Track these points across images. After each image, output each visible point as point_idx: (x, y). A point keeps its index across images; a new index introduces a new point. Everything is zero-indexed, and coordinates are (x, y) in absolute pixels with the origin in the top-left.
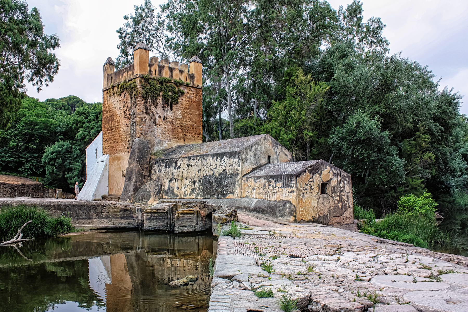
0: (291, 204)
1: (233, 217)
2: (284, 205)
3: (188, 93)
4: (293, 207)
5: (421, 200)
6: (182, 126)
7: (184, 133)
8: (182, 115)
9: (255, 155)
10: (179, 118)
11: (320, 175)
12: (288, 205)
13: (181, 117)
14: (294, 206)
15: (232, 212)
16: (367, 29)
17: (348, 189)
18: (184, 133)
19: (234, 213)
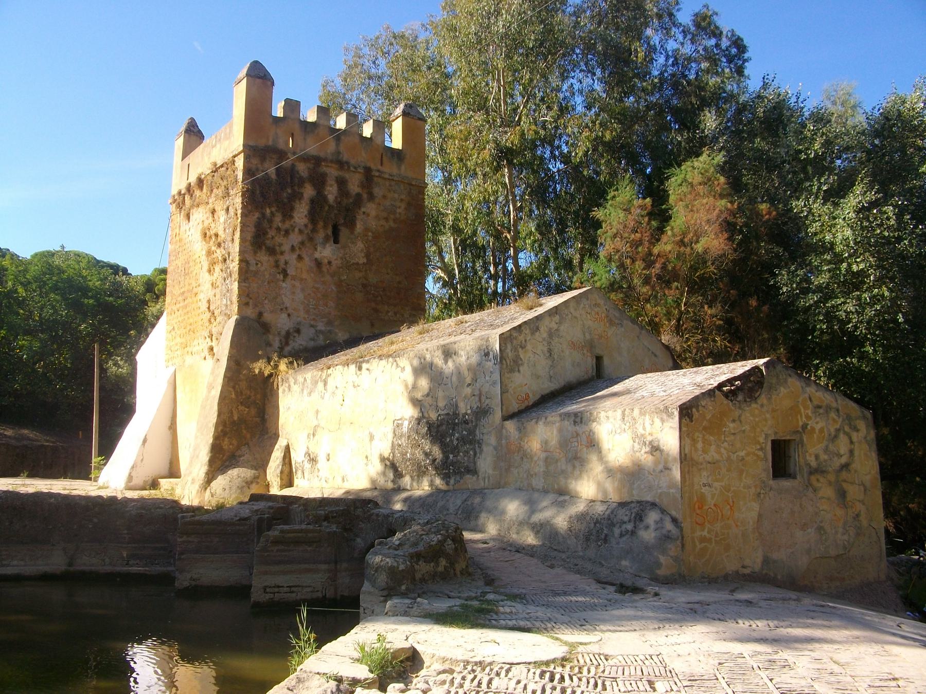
0: (663, 511)
1: (443, 562)
2: (639, 518)
3: (384, 197)
4: (669, 526)
5: (427, 488)
6: (364, 286)
7: (373, 305)
8: (367, 255)
9: (550, 351)
10: (358, 264)
11: (719, 328)
12: (652, 517)
13: (362, 260)
14: (674, 520)
15: (441, 543)
16: (876, 137)
17: (867, 466)
18: (373, 305)
19: (449, 546)
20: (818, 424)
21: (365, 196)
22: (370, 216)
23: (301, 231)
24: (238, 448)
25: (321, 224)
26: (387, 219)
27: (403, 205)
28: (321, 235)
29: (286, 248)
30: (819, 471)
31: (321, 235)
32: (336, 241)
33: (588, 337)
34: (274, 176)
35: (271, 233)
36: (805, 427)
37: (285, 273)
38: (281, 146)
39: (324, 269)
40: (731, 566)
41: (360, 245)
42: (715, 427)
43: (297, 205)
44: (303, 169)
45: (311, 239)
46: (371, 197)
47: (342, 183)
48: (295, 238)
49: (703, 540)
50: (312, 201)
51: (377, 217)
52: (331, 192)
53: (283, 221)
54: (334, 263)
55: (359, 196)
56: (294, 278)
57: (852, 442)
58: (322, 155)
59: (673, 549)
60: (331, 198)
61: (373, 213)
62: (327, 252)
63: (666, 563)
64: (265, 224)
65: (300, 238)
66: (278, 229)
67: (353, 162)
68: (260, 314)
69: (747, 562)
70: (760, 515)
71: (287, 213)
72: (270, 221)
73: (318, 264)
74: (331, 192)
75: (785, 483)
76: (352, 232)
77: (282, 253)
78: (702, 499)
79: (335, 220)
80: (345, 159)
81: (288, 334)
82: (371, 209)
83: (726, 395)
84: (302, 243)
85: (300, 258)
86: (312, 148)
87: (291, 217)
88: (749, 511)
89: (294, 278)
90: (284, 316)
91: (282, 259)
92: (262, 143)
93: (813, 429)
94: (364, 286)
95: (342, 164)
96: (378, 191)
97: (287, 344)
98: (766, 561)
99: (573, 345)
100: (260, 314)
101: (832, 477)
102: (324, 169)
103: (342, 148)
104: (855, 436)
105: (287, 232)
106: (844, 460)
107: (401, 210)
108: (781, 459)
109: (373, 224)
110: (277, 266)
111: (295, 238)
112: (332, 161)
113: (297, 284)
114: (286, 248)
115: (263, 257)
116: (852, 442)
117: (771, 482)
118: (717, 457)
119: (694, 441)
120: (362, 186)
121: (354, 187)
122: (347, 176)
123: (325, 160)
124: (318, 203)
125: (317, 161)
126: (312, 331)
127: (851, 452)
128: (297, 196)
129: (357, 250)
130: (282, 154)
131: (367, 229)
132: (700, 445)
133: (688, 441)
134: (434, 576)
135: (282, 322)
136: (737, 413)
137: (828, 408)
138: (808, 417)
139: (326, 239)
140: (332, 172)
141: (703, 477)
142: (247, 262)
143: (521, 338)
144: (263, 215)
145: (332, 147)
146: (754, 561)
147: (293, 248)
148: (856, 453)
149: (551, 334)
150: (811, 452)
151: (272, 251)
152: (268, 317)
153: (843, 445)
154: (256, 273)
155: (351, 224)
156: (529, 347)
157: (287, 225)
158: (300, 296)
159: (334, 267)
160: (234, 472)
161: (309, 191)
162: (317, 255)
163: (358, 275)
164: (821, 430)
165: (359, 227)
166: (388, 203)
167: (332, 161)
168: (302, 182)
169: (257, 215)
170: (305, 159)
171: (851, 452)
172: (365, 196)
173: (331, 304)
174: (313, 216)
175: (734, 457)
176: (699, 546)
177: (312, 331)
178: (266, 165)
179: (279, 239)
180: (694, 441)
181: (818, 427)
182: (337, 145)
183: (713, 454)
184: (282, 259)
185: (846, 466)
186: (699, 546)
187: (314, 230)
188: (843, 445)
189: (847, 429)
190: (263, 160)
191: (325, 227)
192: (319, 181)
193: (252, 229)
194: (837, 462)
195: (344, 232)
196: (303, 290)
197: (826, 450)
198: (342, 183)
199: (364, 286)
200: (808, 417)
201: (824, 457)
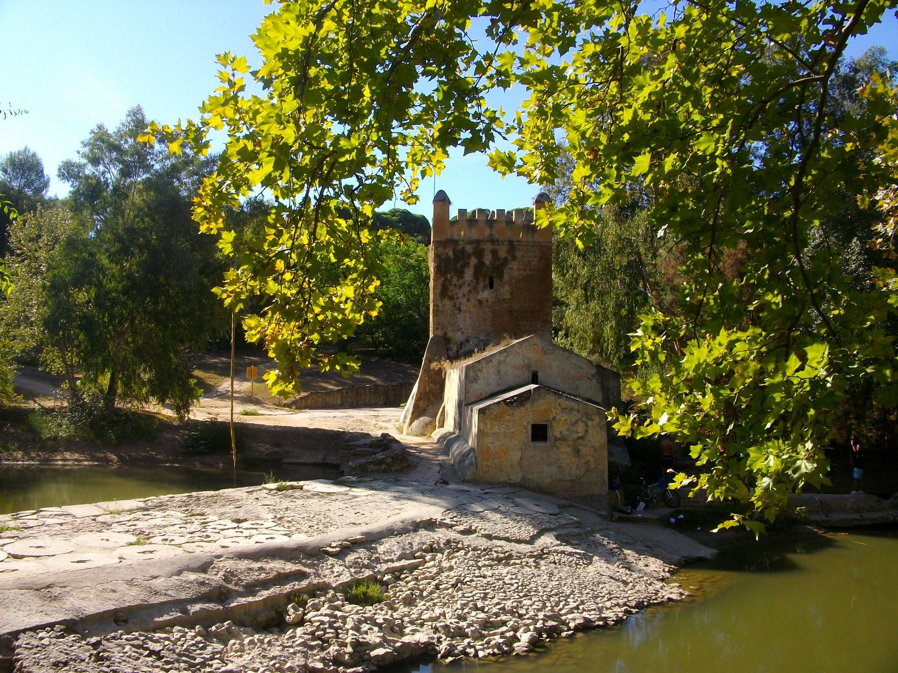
3: (523, 256)
8: (511, 294)
9: (499, 372)
13: (508, 297)
20: (563, 417)
21: (510, 258)
22: (513, 270)
23: (469, 285)
24: (428, 406)
25: (481, 279)
26: (525, 270)
27: (536, 260)
28: (482, 284)
29: (460, 295)
30: (563, 439)
31: (482, 284)
32: (491, 287)
33: (526, 362)
34: (452, 256)
35: (451, 288)
36: (554, 418)
37: (460, 310)
38: (456, 237)
39: (484, 305)
40: (502, 479)
41: (507, 288)
42: (498, 418)
43: (466, 270)
44: (469, 249)
45: (475, 288)
46: (514, 258)
47: (494, 253)
48: (465, 289)
49: (487, 466)
50: (476, 267)
51: (518, 269)
52: (488, 259)
53: (458, 280)
54: (490, 300)
55: (506, 258)
56: (465, 312)
57: (587, 426)
58: (481, 238)
59: (472, 469)
60: (487, 263)
61: (515, 267)
62: (485, 294)
63: (469, 475)
64: (447, 283)
65: (468, 289)
66: (455, 285)
67: (501, 239)
68: (445, 333)
69: (512, 478)
70: (521, 458)
71: (460, 274)
72: (450, 281)
73: (480, 302)
74: (488, 259)
75: (540, 444)
76: (502, 281)
77: (458, 298)
78: (488, 449)
79: (490, 276)
80: (496, 237)
81: (462, 343)
82: (514, 265)
83: (507, 404)
84: (470, 291)
85: (468, 300)
86: (475, 235)
87: (463, 277)
88: (515, 456)
89: (465, 312)
90: (460, 333)
91: (458, 302)
92: (444, 238)
93: (560, 420)
94: (510, 312)
95: (493, 241)
96: (518, 254)
97: (461, 348)
98: (524, 478)
99: (515, 367)
100: (445, 333)
101: (571, 443)
102: (482, 246)
103: (494, 232)
104: (590, 423)
105: (460, 286)
106: (580, 435)
107: (535, 262)
108: (539, 432)
109: (515, 274)
110: (455, 306)
111: (465, 289)
112: (487, 241)
113: (467, 315)
114: (460, 295)
115: (447, 302)
116: (587, 426)
117: (530, 444)
118: (498, 431)
119: (486, 424)
120: (508, 252)
121: (503, 253)
122: (498, 247)
123: (483, 241)
124: (479, 269)
125: (478, 242)
126: (477, 340)
127: (586, 431)
128: (467, 265)
129: (505, 291)
130: (455, 242)
131: (511, 278)
132: (489, 426)
133: (482, 424)
134: (378, 471)
135: (458, 337)
136: (512, 411)
137: (572, 410)
138: (556, 413)
139: (485, 287)
140: (488, 247)
141: (488, 440)
142: (437, 306)
143: (480, 366)
144: (446, 278)
145: (487, 232)
146: (517, 477)
147: (464, 295)
148: (590, 431)
149: (500, 363)
150: (556, 431)
151: (451, 298)
152: (450, 334)
153: (581, 428)
154: (443, 311)
155: (501, 276)
156: (484, 370)
157: (461, 282)
158: (469, 321)
159: (489, 303)
160: (422, 419)
161: (473, 261)
162: (479, 297)
163: (505, 305)
164: (566, 420)
165: (506, 277)
166: (526, 260)
167: (487, 241)
168: (469, 256)
169: (442, 279)
170: (470, 242)
171: (586, 431)
172: (510, 258)
173: (489, 324)
174: (476, 275)
175: (508, 431)
176: (485, 469)
177: (477, 340)
178: (447, 250)
179: (456, 291)
180: (486, 424)
181: (563, 419)
182: (491, 230)
183: (496, 429)
184: (458, 302)
185: (582, 438)
186: (485, 469)
187: (477, 283)
188: (581, 428)
189: (584, 419)
190: (445, 247)
191: (484, 280)
192: (479, 254)
193: (440, 287)
194: (575, 436)
195: (496, 282)
196: (470, 318)
197: (568, 430)
198: (494, 253)
199: (510, 312)
200: (556, 413)
201: (565, 433)
